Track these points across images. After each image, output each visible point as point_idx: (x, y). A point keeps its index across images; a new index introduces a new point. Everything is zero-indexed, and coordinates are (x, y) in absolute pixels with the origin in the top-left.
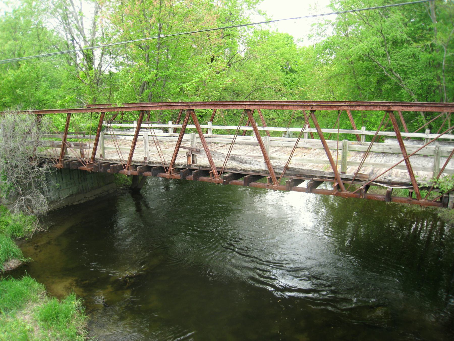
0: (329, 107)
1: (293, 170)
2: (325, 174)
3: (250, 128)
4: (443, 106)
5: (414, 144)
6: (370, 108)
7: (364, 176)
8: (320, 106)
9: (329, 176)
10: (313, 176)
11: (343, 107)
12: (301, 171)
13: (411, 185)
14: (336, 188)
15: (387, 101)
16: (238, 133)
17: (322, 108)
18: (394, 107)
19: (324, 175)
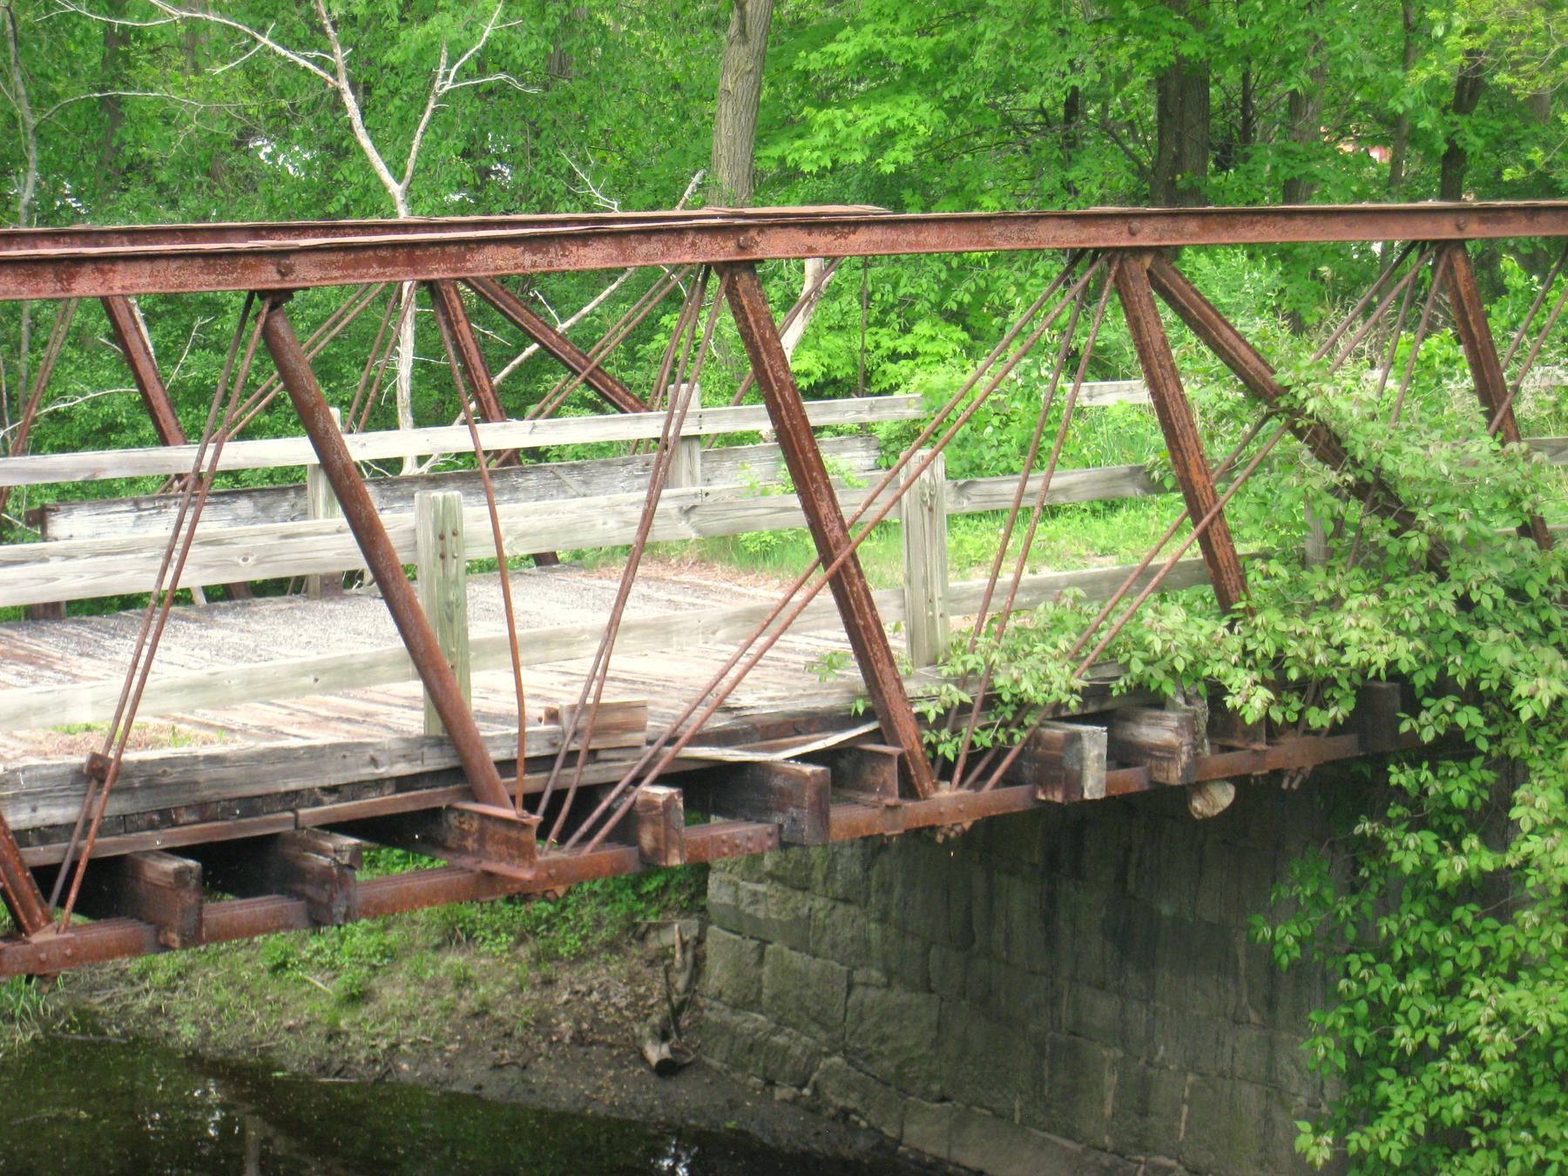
0: (401, 255)
1: (151, 778)
2: (374, 762)
3: (297, 450)
4: (771, 226)
5: (236, 519)
6: (643, 249)
7: (618, 717)
8: (338, 257)
9: (402, 769)
10: (296, 793)
11: (490, 250)
12: (205, 774)
13: (869, 715)
14: (1463, 613)
15: (925, 209)
16: (202, 489)
17: (357, 264)
18: (771, 233)
19: (367, 773)
